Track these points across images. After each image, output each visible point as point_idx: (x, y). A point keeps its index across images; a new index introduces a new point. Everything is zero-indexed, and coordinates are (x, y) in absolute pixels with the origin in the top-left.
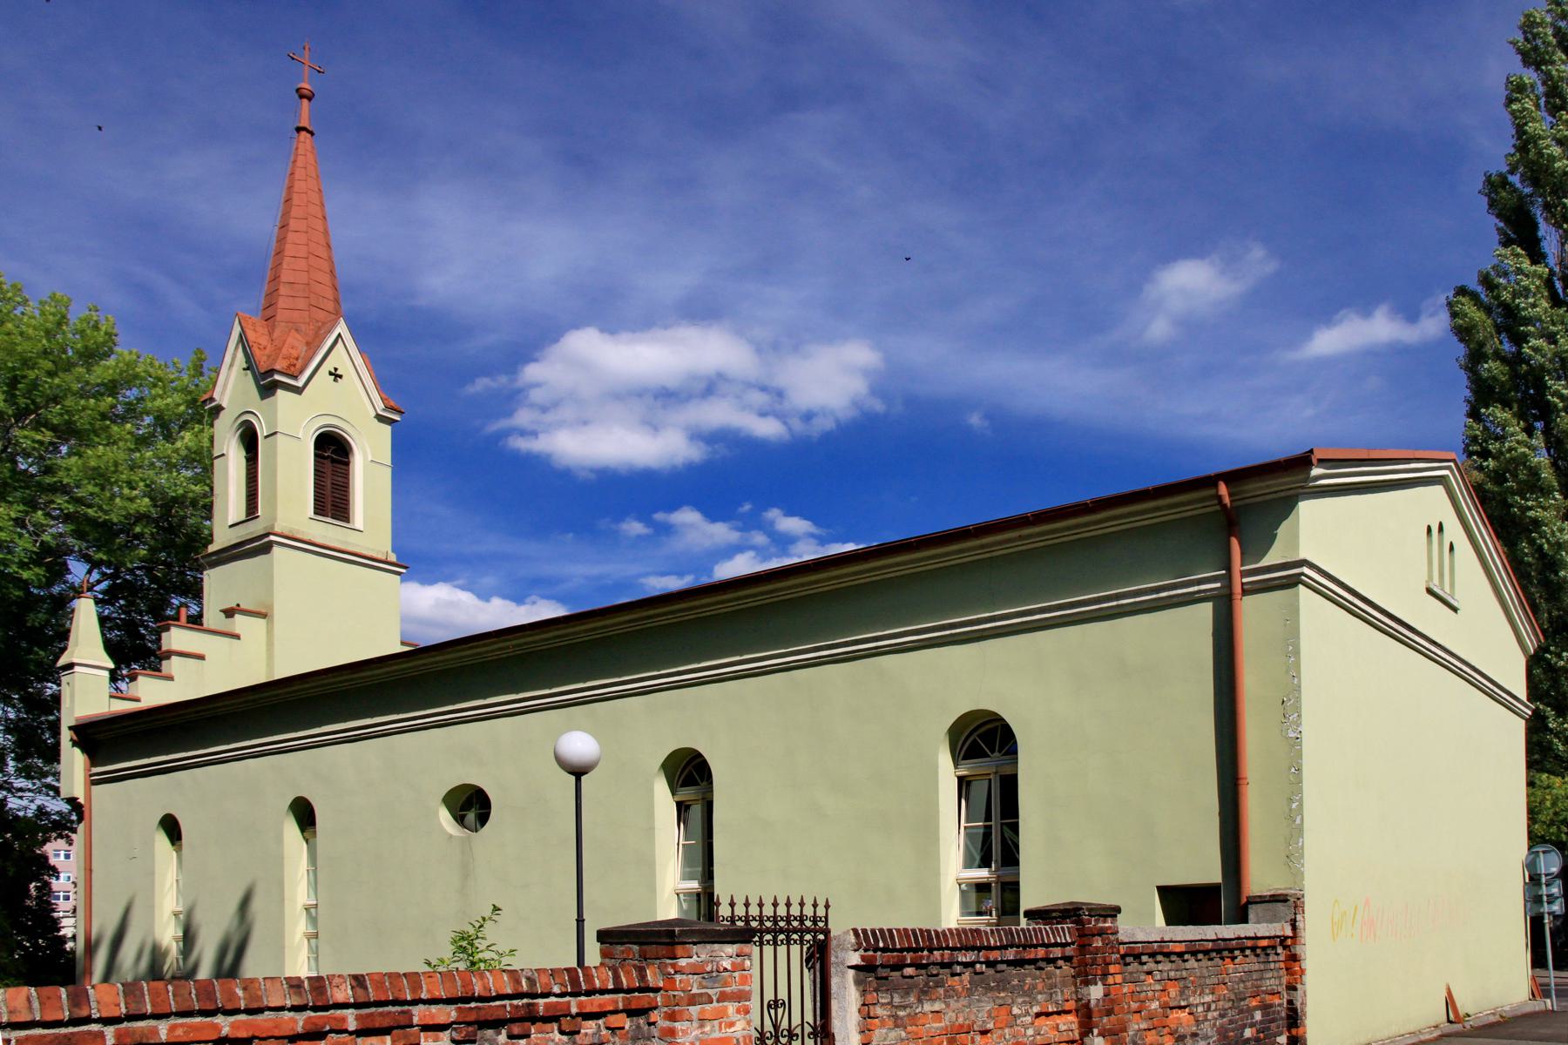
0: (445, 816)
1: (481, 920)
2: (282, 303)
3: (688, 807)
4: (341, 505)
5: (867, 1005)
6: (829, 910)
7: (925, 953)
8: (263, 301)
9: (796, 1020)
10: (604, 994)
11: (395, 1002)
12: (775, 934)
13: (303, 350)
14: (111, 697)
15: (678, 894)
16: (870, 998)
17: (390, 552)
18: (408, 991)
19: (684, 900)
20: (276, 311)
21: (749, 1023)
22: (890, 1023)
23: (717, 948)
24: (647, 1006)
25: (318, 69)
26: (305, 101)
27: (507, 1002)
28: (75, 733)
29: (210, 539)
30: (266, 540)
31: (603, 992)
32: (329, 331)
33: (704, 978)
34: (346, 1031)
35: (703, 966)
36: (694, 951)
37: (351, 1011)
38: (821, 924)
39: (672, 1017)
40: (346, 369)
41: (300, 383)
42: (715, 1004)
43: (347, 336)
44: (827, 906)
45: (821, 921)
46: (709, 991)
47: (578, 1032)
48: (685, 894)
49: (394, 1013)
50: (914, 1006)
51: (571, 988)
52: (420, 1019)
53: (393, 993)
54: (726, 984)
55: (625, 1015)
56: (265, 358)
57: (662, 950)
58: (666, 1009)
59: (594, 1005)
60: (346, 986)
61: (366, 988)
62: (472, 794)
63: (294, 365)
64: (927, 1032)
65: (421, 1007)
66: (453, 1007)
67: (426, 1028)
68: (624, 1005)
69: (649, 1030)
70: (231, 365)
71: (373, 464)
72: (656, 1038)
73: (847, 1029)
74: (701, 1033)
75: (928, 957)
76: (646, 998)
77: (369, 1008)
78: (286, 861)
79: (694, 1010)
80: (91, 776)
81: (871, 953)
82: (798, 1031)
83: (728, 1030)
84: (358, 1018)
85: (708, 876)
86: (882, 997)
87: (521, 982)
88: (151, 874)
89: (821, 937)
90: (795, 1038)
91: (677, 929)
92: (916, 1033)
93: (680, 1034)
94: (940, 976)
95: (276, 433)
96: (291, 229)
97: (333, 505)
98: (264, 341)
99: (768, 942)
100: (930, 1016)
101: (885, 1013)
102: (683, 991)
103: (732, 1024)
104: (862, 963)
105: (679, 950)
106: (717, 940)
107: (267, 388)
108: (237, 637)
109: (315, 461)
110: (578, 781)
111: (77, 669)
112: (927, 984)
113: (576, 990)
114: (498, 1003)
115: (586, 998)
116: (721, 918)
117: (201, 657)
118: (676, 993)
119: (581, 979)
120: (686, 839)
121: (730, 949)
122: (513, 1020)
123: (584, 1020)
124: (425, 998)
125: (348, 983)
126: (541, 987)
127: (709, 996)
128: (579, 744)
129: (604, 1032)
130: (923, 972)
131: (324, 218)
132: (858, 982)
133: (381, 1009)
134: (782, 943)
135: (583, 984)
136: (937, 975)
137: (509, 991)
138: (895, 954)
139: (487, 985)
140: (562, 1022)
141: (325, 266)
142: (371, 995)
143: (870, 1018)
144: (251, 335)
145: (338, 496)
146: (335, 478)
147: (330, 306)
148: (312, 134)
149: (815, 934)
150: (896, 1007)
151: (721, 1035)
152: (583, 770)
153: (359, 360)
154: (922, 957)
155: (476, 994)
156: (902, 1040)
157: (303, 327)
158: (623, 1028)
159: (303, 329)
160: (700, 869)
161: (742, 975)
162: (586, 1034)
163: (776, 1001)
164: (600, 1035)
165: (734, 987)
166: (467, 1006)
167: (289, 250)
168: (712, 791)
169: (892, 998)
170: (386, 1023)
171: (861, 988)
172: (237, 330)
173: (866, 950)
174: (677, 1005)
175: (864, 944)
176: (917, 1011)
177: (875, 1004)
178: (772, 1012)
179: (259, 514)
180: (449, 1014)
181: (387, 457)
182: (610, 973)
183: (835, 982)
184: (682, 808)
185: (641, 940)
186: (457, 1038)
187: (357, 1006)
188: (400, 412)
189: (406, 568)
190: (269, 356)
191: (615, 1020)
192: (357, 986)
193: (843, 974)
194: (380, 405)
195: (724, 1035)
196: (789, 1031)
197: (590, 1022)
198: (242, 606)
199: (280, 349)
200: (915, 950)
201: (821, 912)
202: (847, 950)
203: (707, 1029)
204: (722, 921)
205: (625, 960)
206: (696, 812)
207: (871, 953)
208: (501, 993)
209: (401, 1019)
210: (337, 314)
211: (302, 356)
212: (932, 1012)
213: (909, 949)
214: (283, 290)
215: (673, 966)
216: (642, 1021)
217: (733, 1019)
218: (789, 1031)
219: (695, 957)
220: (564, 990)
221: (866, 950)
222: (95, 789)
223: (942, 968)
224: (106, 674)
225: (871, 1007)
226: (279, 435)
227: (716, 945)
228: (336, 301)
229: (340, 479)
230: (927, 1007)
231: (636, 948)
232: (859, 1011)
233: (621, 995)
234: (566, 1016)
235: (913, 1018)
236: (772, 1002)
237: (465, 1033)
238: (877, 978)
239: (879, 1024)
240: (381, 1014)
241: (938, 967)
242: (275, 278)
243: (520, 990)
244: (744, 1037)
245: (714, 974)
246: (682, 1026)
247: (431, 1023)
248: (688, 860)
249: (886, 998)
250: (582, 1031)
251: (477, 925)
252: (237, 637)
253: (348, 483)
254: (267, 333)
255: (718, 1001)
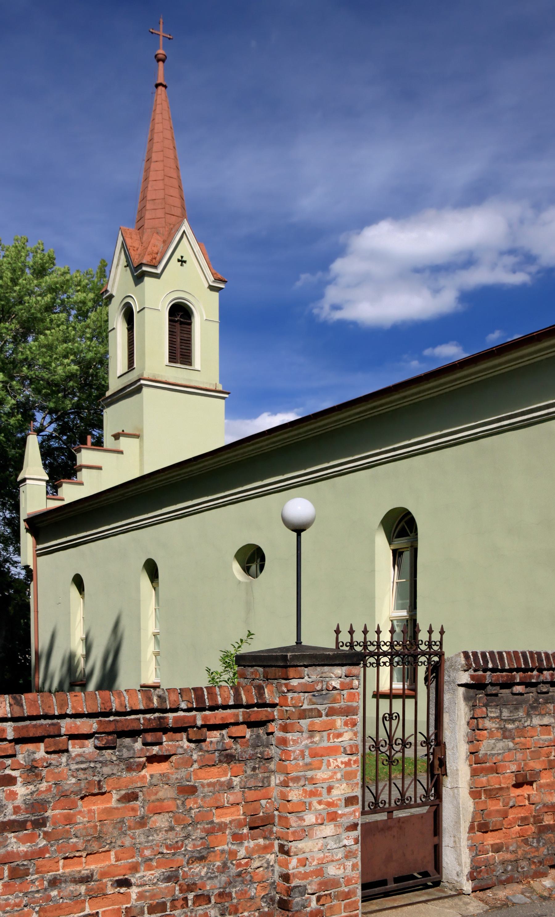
0: (236, 567)
1: (239, 642)
2: (148, 215)
3: (401, 553)
4: (186, 354)
5: (476, 718)
6: (444, 636)
7: (535, 673)
8: (137, 217)
9: (410, 730)
10: (226, 709)
11: (46, 717)
12: (378, 657)
13: (160, 245)
14: (47, 498)
15: (392, 621)
16: (479, 713)
17: (218, 383)
18: (56, 707)
19: (397, 625)
20: (144, 222)
21: (355, 734)
22: (499, 735)
23: (326, 670)
24: (264, 719)
25: (169, 36)
26: (161, 63)
27: (141, 716)
28: (27, 524)
29: (107, 388)
30: (138, 384)
31: (225, 707)
32: (177, 230)
33: (314, 696)
34: (5, 740)
35: (313, 685)
36: (306, 672)
37: (9, 723)
38: (436, 648)
39: (285, 729)
40: (189, 257)
41: (159, 271)
42: (324, 718)
43: (189, 232)
44: (442, 632)
45: (435, 644)
46: (319, 707)
47: (204, 741)
48: (398, 621)
49: (46, 725)
50: (523, 720)
51: (197, 704)
52: (67, 730)
53: (43, 710)
54: (335, 701)
55: (246, 726)
56: (137, 256)
57: (279, 672)
58: (280, 722)
59: (217, 719)
60: (6, 704)
61: (22, 706)
62: (254, 552)
63: (155, 258)
64: (535, 743)
65: (68, 720)
66: (95, 720)
67: (72, 737)
68: (243, 718)
69: (268, 739)
70: (118, 265)
71: (207, 322)
72: (274, 746)
73: (456, 739)
74: (311, 743)
75: (538, 677)
76: (264, 713)
77: (24, 721)
78: (142, 603)
79: (304, 723)
80: (36, 551)
81: (480, 673)
82: (412, 740)
83: (335, 740)
84: (15, 729)
85: (413, 607)
86: (491, 712)
87: (153, 700)
88: (68, 614)
89: (436, 659)
90: (408, 746)
91: (289, 654)
92: (524, 744)
93: (291, 743)
94: (550, 694)
95: (144, 308)
96: (153, 160)
97: (181, 355)
98: (137, 244)
99: (385, 663)
100: (539, 729)
101: (494, 725)
102: (294, 707)
103: (340, 735)
104: (472, 682)
105: (292, 672)
106: (326, 663)
107: (139, 278)
108: (121, 452)
109: (169, 324)
110: (299, 535)
111: (28, 482)
112: (536, 700)
113: (201, 706)
114: (133, 717)
115: (210, 712)
116: (341, 644)
117: (100, 468)
118: (288, 708)
119: (206, 697)
120: (399, 578)
121: (339, 671)
122: (146, 731)
123: (208, 730)
124: (70, 713)
125: (7, 702)
126: (170, 704)
127: (319, 711)
128: (299, 508)
129: (227, 740)
130: (533, 689)
131: (174, 148)
132: (467, 699)
133: (34, 722)
134: (398, 664)
135: (207, 701)
136: (547, 693)
137: (142, 707)
138: (504, 674)
139: (123, 702)
140: (190, 732)
141: (176, 184)
142: (25, 711)
143: (479, 730)
144: (129, 242)
145: (185, 348)
146: (182, 335)
147: (178, 211)
148: (165, 87)
149: (430, 656)
150: (505, 721)
151: (329, 744)
152: (302, 528)
153: (197, 248)
154: (532, 677)
155: (114, 710)
156: (510, 750)
157: (161, 230)
158: (244, 737)
159: (161, 232)
160: (408, 601)
161: (351, 693)
162: (211, 742)
163: (391, 714)
164: (223, 743)
165: (342, 703)
166: (107, 719)
167: (152, 176)
168: (417, 540)
169: (501, 712)
170: (39, 733)
171: (471, 704)
172: (120, 239)
173: (475, 671)
174: (289, 718)
175: (474, 665)
176: (526, 724)
177: (485, 717)
178: (387, 724)
179: (135, 366)
180: (91, 726)
181: (216, 317)
182: (232, 692)
183: (447, 697)
184: (397, 554)
185: (265, 664)
186: (98, 745)
187: (14, 719)
188: (224, 282)
189: (228, 393)
190: (140, 255)
191: (236, 731)
192: (15, 704)
193: (454, 691)
194: (211, 278)
195: (332, 745)
196: (403, 740)
197: (215, 732)
198: (126, 432)
199: (147, 248)
200: (525, 670)
201: (436, 637)
202: (457, 670)
203: (317, 739)
204: (342, 646)
205: (254, 679)
206: (407, 556)
207: (480, 673)
208: (134, 708)
209: (51, 729)
210: (183, 216)
211: (160, 251)
212: (541, 726)
213: (518, 670)
214: (148, 206)
215: (286, 685)
216: (261, 731)
217: (341, 731)
218: (403, 740)
219: (306, 678)
220: (190, 706)
221: (475, 671)
222: (40, 559)
223: (551, 686)
224: (44, 484)
225: (480, 720)
226: (146, 309)
227: (326, 667)
228: (183, 208)
229: (185, 335)
230: (536, 721)
231: (261, 669)
232: (468, 723)
233: (242, 710)
234: (193, 727)
235: (522, 731)
236: (387, 715)
237: (105, 741)
238: (487, 695)
239: (487, 735)
240: (35, 726)
241: (548, 685)
242: (144, 198)
243: (151, 706)
244: (350, 746)
245: (324, 692)
246: (293, 736)
247: (76, 733)
248: (400, 595)
249: (495, 712)
250: (208, 740)
251: (237, 646)
252: (121, 452)
253: (190, 338)
254: (139, 239)
255: (327, 715)
